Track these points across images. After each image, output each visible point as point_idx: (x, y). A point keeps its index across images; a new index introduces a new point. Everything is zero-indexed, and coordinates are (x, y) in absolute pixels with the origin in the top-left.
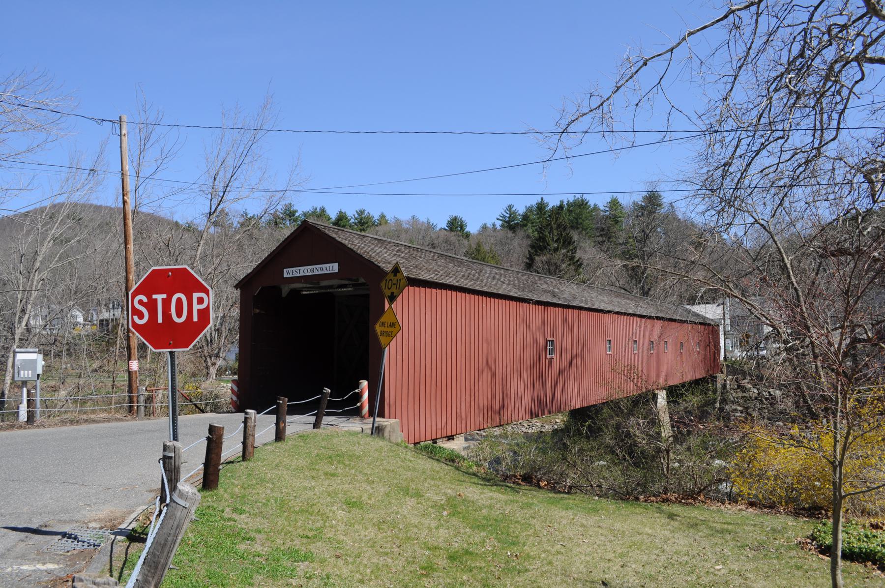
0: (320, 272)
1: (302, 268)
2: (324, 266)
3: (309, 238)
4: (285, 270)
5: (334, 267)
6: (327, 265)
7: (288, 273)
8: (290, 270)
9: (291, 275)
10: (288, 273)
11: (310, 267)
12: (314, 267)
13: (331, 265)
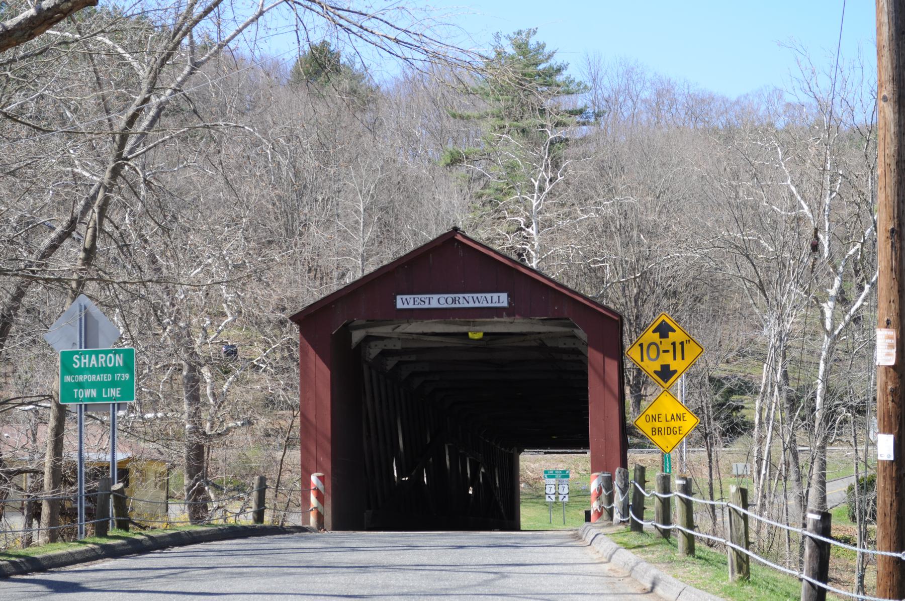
1: (436, 297)
3: (450, 259)
4: (399, 298)
5: (501, 300)
7: (404, 302)
10: (404, 302)
13: (495, 296)
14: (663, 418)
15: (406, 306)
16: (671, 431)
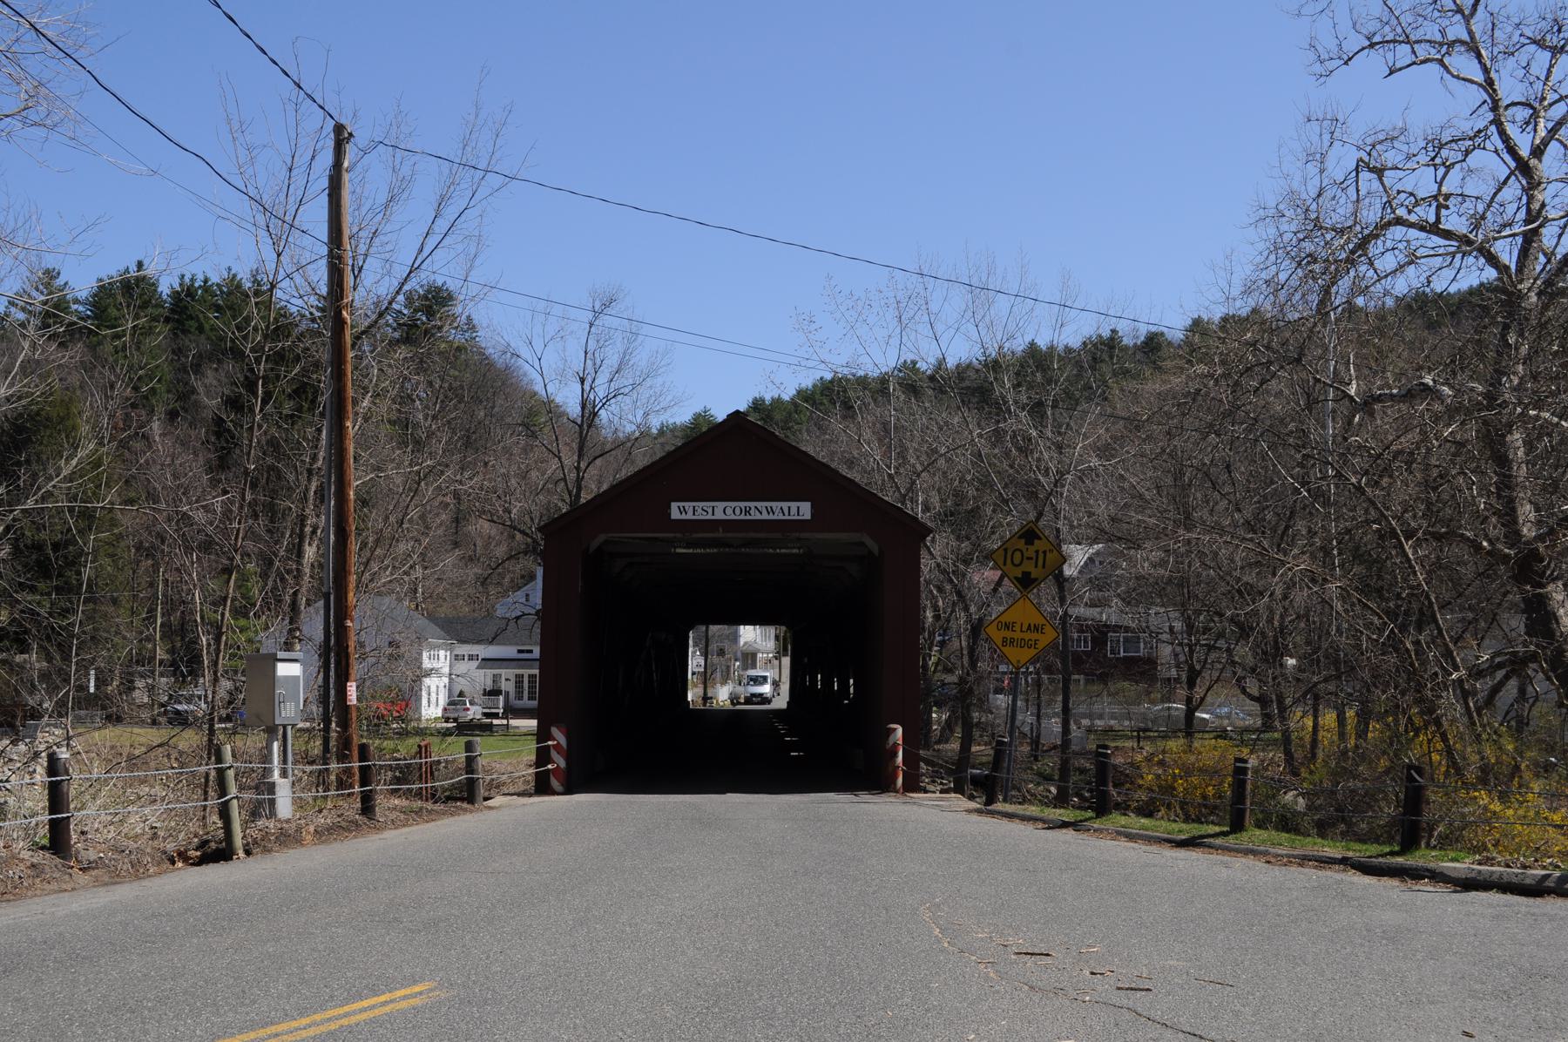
0: (765, 516)
1: (720, 505)
2: (775, 505)
4: (674, 505)
5: (805, 510)
6: (785, 505)
8: (688, 505)
9: (690, 516)
11: (743, 504)
12: (752, 504)
13: (794, 505)
14: (1017, 628)
15: (684, 517)
16: (1024, 644)
